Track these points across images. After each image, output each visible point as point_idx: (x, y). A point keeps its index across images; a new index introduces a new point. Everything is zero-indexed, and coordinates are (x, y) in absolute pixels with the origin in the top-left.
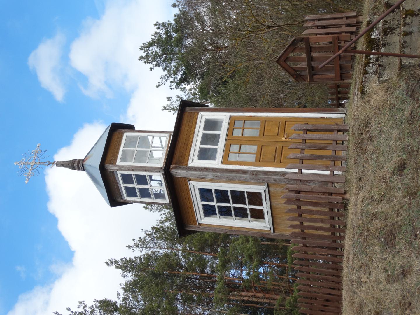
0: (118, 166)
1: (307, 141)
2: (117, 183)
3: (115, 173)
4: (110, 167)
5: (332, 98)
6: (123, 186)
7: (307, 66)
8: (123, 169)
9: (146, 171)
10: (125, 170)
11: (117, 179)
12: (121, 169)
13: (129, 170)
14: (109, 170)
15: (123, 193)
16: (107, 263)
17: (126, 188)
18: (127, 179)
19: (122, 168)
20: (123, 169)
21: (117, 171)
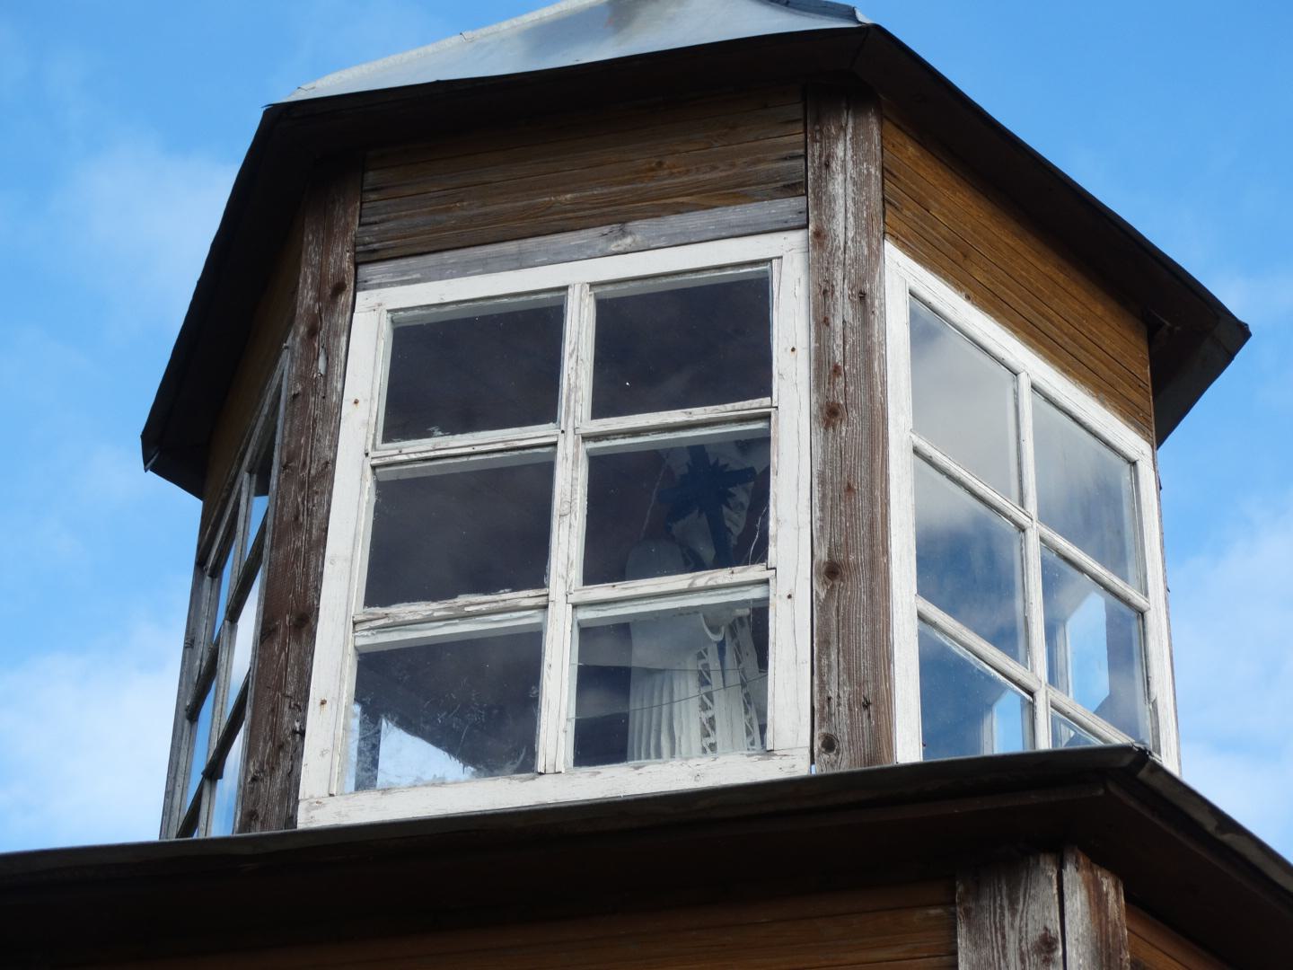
0: (876, 256)
1: (576, 426)
2: (615, 214)
3: (788, 206)
4: (850, 163)
5: (725, 645)
6: (578, 276)
7: (908, 748)
8: (843, 310)
9: (831, 572)
10: (821, 321)
11: (674, 222)
12: (842, 288)
13: (825, 371)
14: (815, 150)
15: (486, 267)
16: (443, 295)
17: (543, 319)
18: (708, 338)
19: (846, 304)
20: (843, 310)
21: (797, 238)
